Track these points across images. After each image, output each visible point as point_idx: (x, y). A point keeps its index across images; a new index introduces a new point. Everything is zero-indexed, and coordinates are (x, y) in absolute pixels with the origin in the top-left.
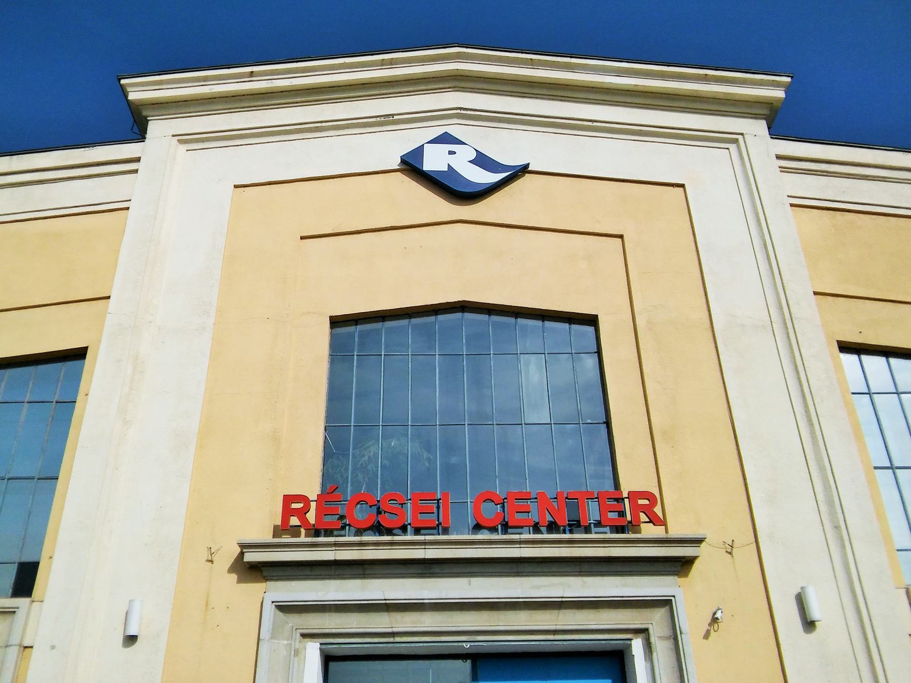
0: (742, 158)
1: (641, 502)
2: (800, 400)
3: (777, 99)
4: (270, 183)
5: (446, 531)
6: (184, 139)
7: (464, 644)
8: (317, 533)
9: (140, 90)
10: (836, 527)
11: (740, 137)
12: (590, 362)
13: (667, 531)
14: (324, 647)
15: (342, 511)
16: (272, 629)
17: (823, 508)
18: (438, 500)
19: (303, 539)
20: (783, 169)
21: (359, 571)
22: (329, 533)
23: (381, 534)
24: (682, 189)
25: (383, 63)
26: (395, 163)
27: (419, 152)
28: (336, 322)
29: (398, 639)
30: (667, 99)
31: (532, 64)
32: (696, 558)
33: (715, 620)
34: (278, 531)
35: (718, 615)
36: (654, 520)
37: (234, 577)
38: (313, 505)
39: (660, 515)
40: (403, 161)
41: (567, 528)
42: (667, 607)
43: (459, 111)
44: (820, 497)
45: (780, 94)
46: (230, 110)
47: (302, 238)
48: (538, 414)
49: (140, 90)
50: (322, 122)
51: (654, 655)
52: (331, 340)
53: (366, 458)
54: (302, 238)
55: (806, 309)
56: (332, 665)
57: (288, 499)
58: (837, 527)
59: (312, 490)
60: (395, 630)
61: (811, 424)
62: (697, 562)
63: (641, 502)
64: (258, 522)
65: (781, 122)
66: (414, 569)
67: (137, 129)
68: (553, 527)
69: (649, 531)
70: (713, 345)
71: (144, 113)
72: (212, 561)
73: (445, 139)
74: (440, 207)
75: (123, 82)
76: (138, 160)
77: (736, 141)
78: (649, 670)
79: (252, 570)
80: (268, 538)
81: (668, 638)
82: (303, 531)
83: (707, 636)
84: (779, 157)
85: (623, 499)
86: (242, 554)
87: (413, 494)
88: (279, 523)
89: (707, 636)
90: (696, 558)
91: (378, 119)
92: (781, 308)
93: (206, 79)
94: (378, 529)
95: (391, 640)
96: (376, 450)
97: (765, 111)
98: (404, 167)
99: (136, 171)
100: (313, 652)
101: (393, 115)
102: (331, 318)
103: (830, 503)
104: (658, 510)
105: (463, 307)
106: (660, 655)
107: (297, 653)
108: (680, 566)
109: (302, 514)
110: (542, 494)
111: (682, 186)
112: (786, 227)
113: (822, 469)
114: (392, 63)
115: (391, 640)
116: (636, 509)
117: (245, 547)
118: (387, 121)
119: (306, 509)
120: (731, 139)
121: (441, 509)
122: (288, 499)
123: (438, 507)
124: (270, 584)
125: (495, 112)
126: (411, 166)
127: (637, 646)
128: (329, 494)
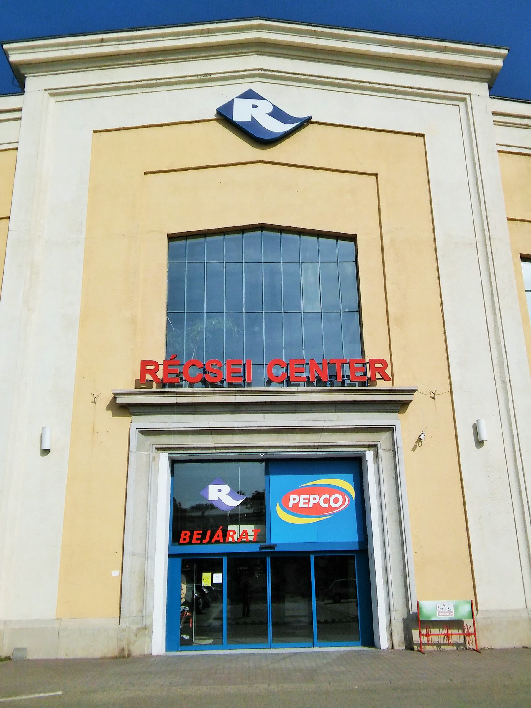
0: (467, 114)
1: (377, 366)
2: (490, 296)
3: (497, 67)
4: (119, 129)
5: (249, 385)
6: (55, 93)
7: (260, 454)
8: (164, 386)
9: (18, 53)
10: (503, 382)
11: (468, 97)
12: (350, 268)
13: (393, 385)
14: (171, 455)
15: (181, 369)
16: (137, 445)
17: (496, 369)
18: (244, 365)
19: (154, 389)
20: (496, 123)
21: (192, 409)
22: (172, 386)
23: (206, 386)
24: (422, 138)
25: (202, 32)
26: (212, 114)
27: (230, 105)
28: (171, 238)
29: (218, 451)
30: (418, 65)
31: (315, 34)
32: (411, 401)
33: (420, 440)
34: (138, 384)
35: (422, 437)
36: (385, 377)
37: (110, 413)
38: (161, 367)
39: (390, 375)
40: (219, 113)
41: (328, 383)
42: (391, 432)
43: (260, 72)
44: (495, 362)
45: (499, 63)
46: (87, 69)
47: (145, 173)
48: (312, 304)
49: (18, 53)
50: (156, 79)
51: (380, 460)
52: (169, 251)
53: (196, 332)
54: (145, 173)
55: (500, 230)
56: (176, 465)
57: (144, 364)
58: (504, 382)
59: (160, 358)
60: (216, 445)
61: (494, 311)
62: (411, 404)
63: (377, 366)
64: (125, 379)
65: (500, 86)
66: (228, 409)
67: (18, 87)
68: (319, 381)
69: (381, 384)
70: (435, 258)
71: (22, 71)
72: (95, 403)
73: (250, 95)
74: (247, 151)
75: (5, 46)
76: (21, 110)
77: (464, 100)
78: (382, 547)
79: (122, 409)
80: (131, 388)
81: (390, 450)
82: (155, 384)
83: (414, 449)
84: (494, 113)
85: (366, 364)
86: (115, 398)
87: (227, 361)
88: (139, 378)
89: (414, 449)
90: (411, 401)
91: (199, 77)
92: (483, 230)
93: (67, 44)
94: (205, 383)
95: (214, 451)
96: (202, 326)
97: (489, 77)
98: (219, 117)
99: (20, 119)
100: (164, 459)
101: (210, 74)
102: (168, 235)
103: (501, 366)
104: (388, 371)
105: (262, 227)
106: (384, 463)
107: (154, 459)
108: (401, 406)
109: (154, 373)
110: (313, 361)
111: (423, 135)
112: (493, 167)
113: (498, 343)
114: (209, 32)
115: (214, 451)
116: (374, 370)
117: (116, 394)
118: (206, 79)
119: (157, 370)
120: (461, 98)
121: (246, 371)
122: (144, 364)
123: (244, 369)
124: (134, 417)
125: (287, 73)
126: (224, 116)
127: (370, 455)
128: (171, 360)
